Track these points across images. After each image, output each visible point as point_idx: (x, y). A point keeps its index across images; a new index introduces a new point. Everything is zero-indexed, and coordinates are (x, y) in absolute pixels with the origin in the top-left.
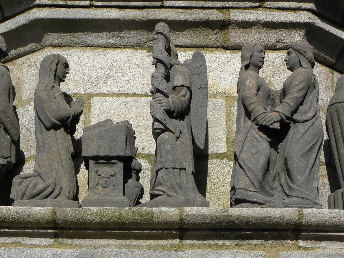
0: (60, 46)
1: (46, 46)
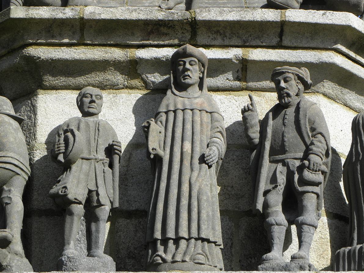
0: (329, 97)
1: (318, 92)
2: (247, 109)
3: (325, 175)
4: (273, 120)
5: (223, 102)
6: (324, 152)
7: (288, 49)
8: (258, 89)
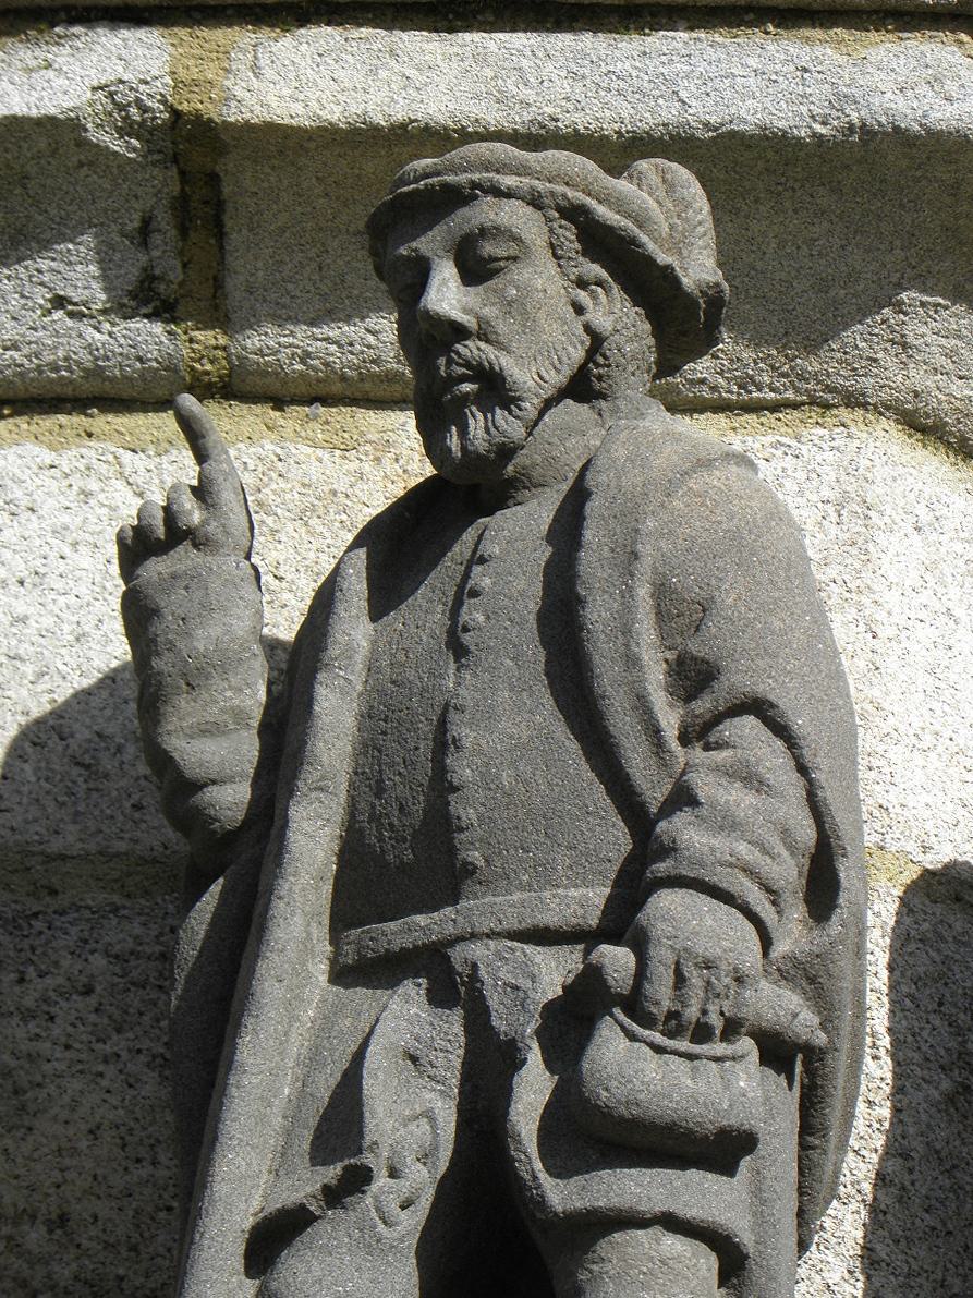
1: (854, 400)
2: (161, 532)
3: (809, 1071)
4: (376, 614)
5: (25, 502)
6: (788, 871)
7: (571, 29)
8: (337, 388)
